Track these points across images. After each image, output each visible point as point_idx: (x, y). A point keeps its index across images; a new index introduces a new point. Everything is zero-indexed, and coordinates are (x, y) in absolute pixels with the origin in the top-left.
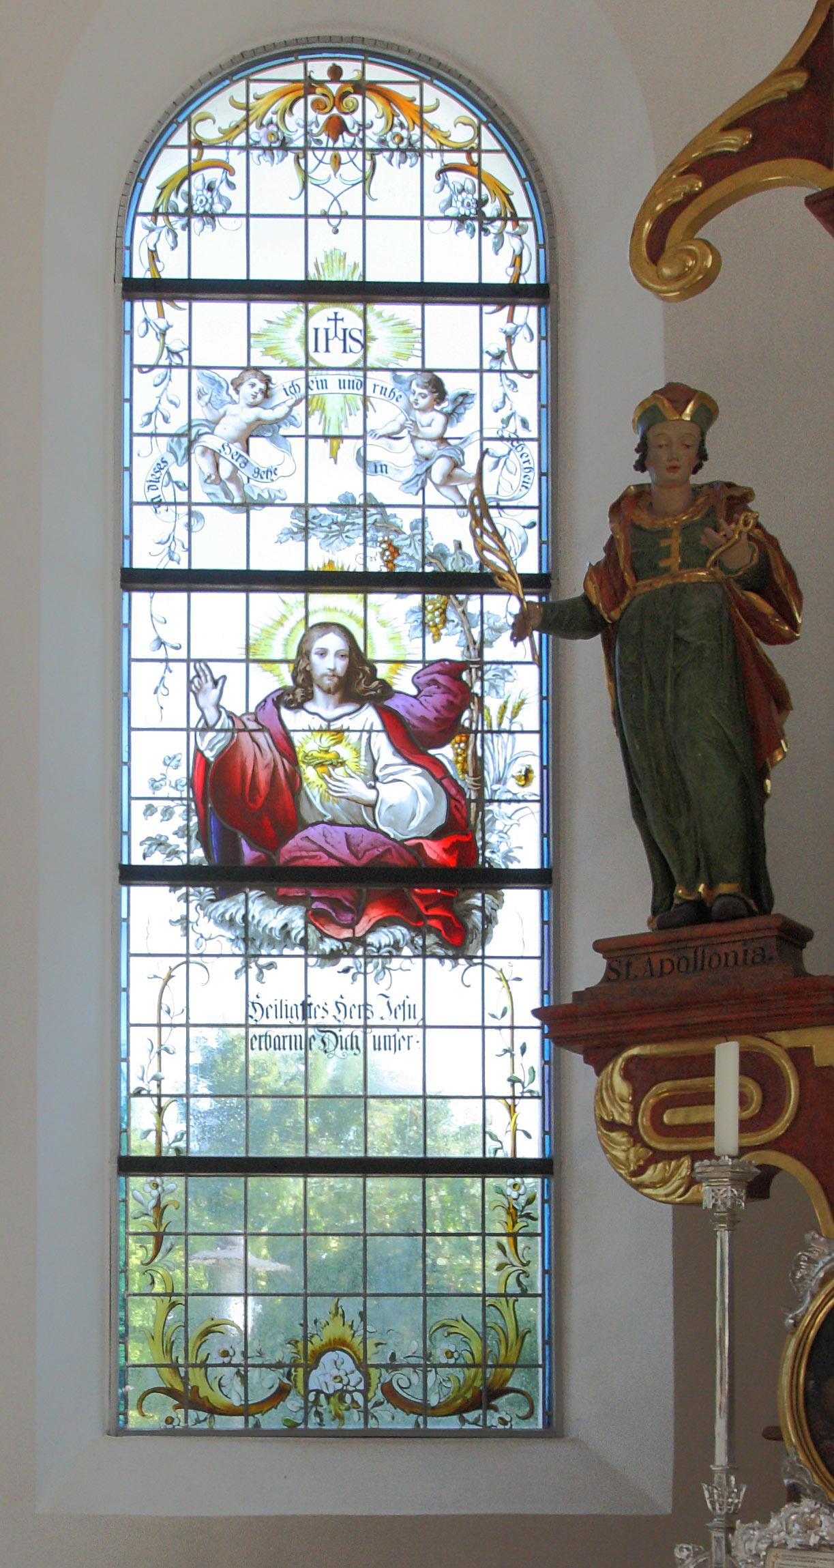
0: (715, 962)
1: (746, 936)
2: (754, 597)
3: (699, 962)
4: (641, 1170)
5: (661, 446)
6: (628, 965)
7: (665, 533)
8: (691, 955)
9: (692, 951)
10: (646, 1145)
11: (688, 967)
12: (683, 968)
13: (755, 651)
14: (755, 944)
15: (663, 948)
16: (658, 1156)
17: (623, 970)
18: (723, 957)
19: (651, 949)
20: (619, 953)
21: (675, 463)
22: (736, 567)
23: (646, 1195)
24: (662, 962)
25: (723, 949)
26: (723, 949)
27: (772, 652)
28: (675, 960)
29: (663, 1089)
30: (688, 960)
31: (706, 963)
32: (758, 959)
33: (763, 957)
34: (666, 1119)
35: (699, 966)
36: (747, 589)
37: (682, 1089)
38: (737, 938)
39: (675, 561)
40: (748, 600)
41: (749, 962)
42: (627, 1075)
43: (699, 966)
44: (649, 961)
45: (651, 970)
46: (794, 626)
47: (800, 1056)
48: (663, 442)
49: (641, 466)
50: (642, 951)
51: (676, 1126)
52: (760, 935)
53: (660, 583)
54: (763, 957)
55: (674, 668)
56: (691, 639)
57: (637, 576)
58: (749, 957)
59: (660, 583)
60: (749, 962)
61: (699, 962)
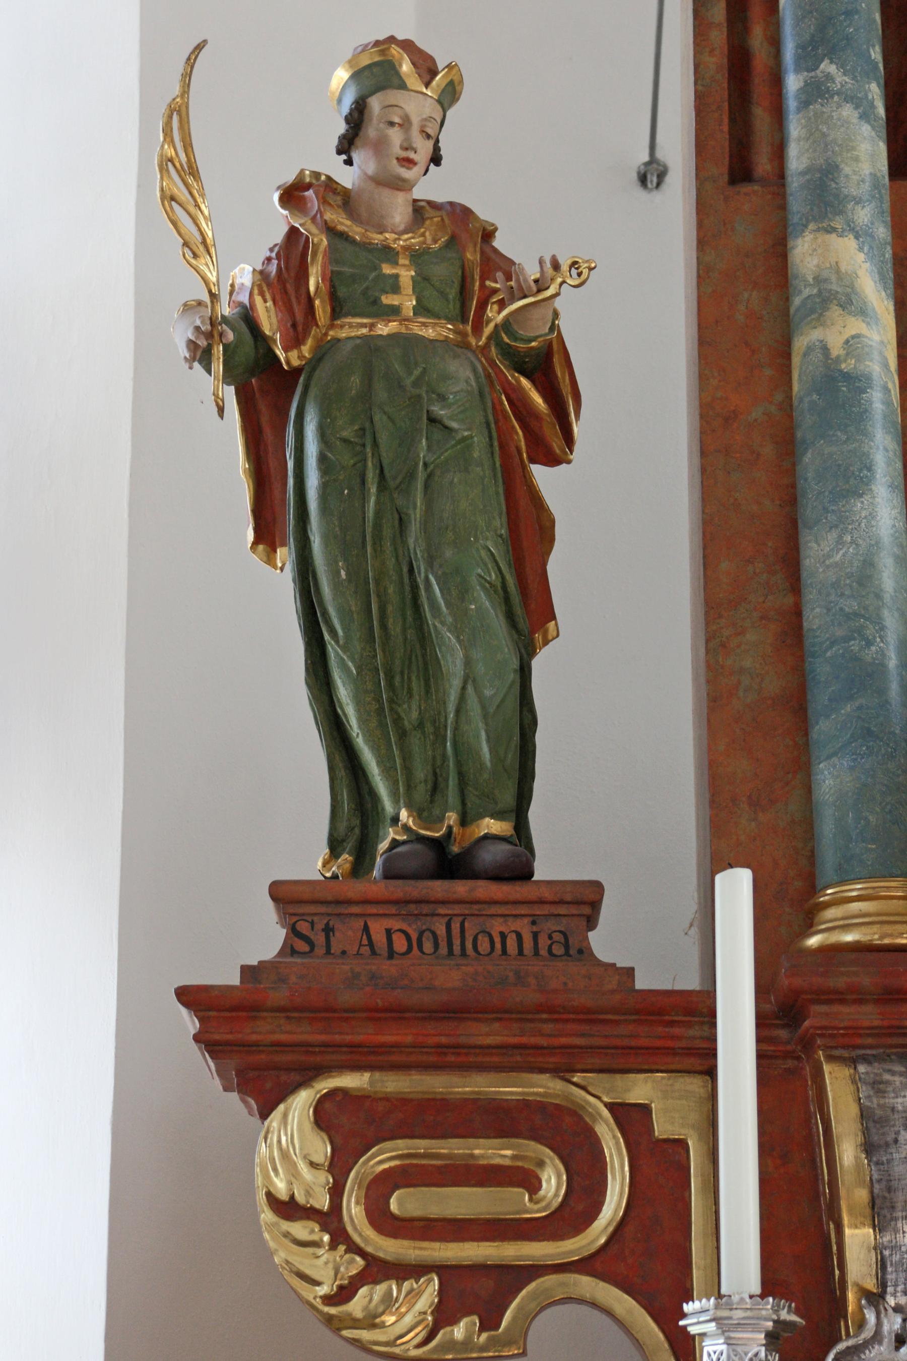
0: (484, 946)
1: (538, 910)
2: (524, 382)
3: (457, 943)
4: (344, 1294)
5: (392, 124)
6: (328, 930)
7: (388, 253)
8: (441, 931)
9: (444, 921)
10: (354, 1249)
11: (436, 946)
12: (428, 946)
13: (524, 467)
14: (551, 925)
15: (393, 910)
16: (377, 1270)
17: (319, 939)
18: (497, 940)
19: (373, 910)
20: (312, 909)
21: (412, 155)
22: (532, 334)
23: (347, 1339)
24: (389, 932)
25: (497, 927)
26: (497, 927)
27: (539, 473)
28: (414, 936)
29: (381, 1159)
30: (434, 934)
31: (469, 945)
32: (558, 950)
33: (567, 946)
34: (394, 1206)
35: (457, 948)
36: (520, 372)
37: (425, 1156)
38: (523, 910)
39: (409, 303)
40: (519, 388)
41: (543, 952)
42: (323, 1117)
43: (457, 948)
44: (366, 929)
45: (371, 944)
46: (569, 439)
47: (632, 1118)
48: (397, 120)
49: (346, 146)
50: (355, 909)
51: (412, 1220)
52: (562, 910)
53: (384, 329)
54: (567, 946)
55: (426, 465)
56: (454, 425)
57: (337, 310)
58: (543, 942)
59: (384, 329)
60: (543, 952)
61: (457, 943)
